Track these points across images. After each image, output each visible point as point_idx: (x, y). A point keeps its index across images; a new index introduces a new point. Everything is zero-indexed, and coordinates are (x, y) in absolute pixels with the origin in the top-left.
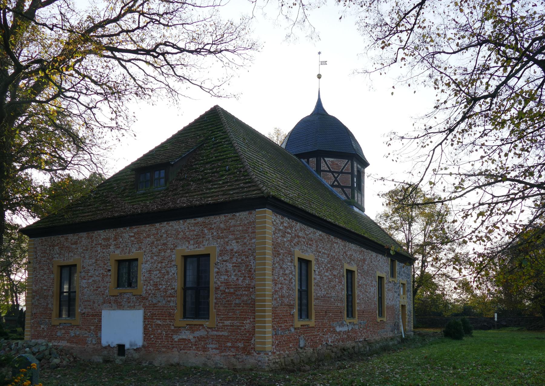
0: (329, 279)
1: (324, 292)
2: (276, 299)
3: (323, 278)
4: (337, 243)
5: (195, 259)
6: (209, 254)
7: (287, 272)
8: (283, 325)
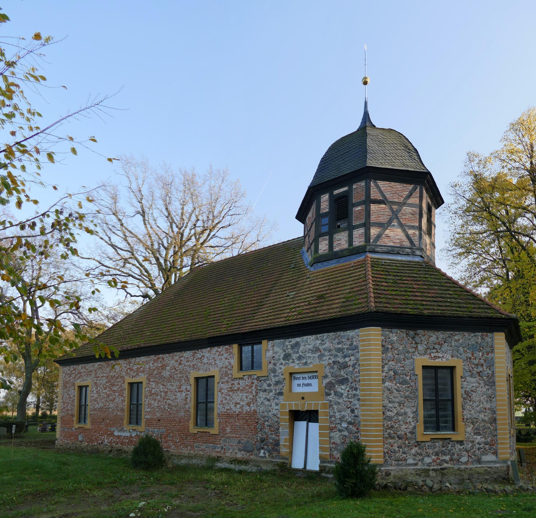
0: (106, 394)
1: (101, 405)
2: (64, 412)
3: (100, 395)
4: (119, 364)
5: (433, 371)
6: (214, 376)
7: (71, 396)
8: (68, 426)
